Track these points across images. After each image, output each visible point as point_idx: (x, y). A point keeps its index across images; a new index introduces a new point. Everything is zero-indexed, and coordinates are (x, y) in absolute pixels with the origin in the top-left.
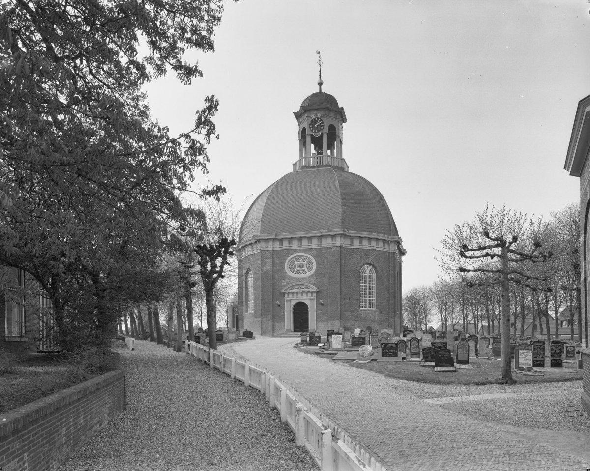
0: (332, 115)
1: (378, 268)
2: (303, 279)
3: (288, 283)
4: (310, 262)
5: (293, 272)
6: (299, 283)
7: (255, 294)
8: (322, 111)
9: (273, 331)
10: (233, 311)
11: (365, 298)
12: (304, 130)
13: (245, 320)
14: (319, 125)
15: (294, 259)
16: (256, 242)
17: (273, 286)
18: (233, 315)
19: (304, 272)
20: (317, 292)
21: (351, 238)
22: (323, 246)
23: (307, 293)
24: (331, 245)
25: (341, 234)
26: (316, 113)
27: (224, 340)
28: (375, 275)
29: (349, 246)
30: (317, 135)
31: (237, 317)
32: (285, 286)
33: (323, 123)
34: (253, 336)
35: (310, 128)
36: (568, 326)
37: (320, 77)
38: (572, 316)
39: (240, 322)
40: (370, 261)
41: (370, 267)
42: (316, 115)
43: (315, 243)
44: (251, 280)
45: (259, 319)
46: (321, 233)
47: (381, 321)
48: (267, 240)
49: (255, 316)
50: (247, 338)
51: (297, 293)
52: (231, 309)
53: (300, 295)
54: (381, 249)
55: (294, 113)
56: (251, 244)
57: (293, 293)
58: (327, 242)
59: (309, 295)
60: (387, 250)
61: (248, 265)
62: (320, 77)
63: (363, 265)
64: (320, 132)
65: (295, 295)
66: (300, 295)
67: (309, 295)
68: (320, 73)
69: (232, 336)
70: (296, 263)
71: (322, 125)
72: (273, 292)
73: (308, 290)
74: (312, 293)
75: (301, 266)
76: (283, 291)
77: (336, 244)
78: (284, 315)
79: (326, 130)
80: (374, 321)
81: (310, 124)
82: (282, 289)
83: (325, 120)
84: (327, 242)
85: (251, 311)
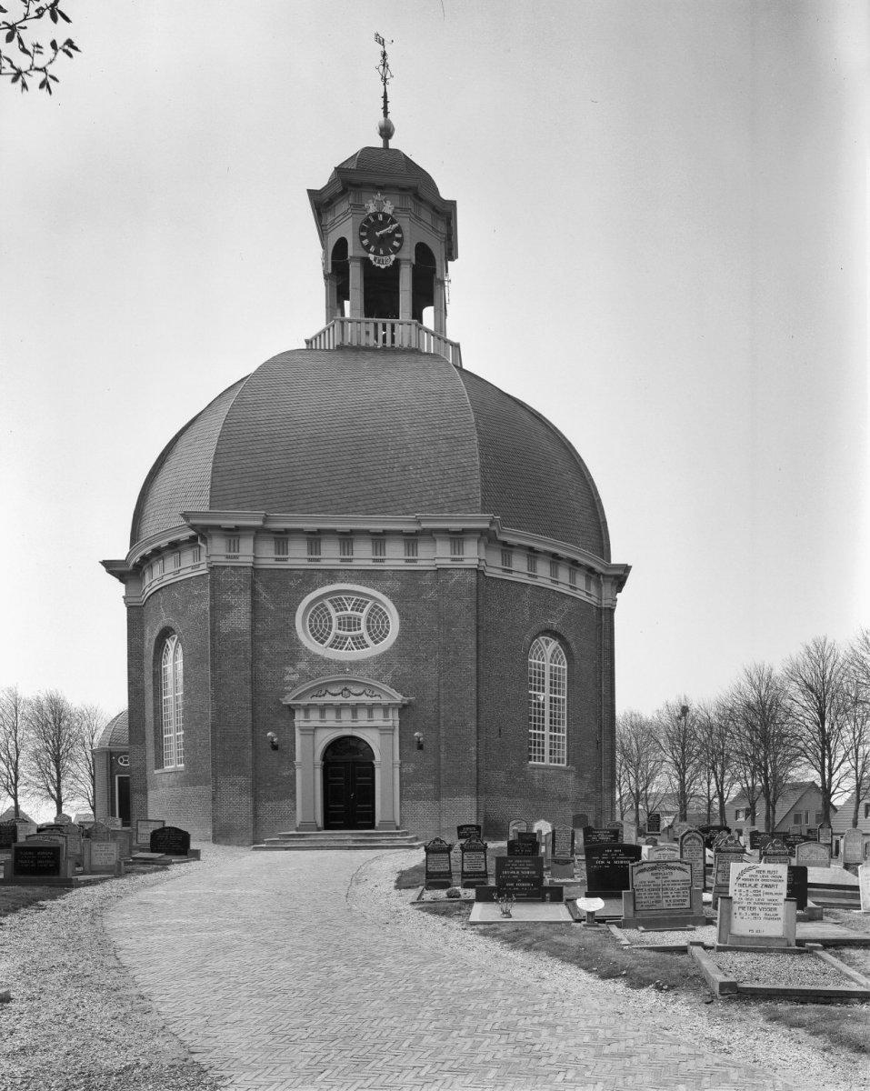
0: (426, 215)
1: (573, 646)
2: (356, 665)
3: (306, 676)
4: (377, 616)
5: (322, 642)
6: (345, 677)
7: (188, 709)
8: (397, 197)
9: (256, 826)
10: (112, 767)
11: (541, 732)
12: (341, 245)
13: (151, 794)
14: (390, 236)
15: (371, 602)
16: (193, 540)
17: (254, 681)
18: (111, 778)
19: (359, 643)
20: (403, 709)
21: (507, 549)
22: (422, 564)
23: (370, 708)
24: (447, 563)
25: (482, 532)
26: (378, 197)
27: (68, 868)
28: (566, 667)
29: (497, 574)
30: (385, 262)
31: (125, 784)
32: (295, 686)
33: (398, 230)
34: (193, 846)
35: (362, 238)
36: (746, 819)
37: (386, 113)
38: (753, 804)
39: (136, 799)
40: (554, 623)
41: (554, 644)
42: (380, 204)
43: (395, 555)
44: (174, 664)
45: (206, 790)
46: (419, 522)
47: (582, 800)
48: (234, 533)
49: (190, 778)
50: (168, 853)
51: (338, 709)
52: (102, 761)
53: (346, 715)
54: (582, 596)
55: (310, 192)
56: (175, 546)
57: (323, 709)
58: (435, 555)
59: (378, 715)
60: (593, 600)
61: (166, 619)
62: (386, 113)
63: (536, 637)
64: (393, 257)
65: (330, 715)
66: (346, 715)
67: (378, 715)
68: (386, 102)
69: (105, 853)
70: (334, 615)
71: (397, 235)
72: (254, 704)
73: (376, 700)
74: (386, 708)
75: (350, 623)
76: (288, 700)
77: (466, 562)
78: (293, 777)
79: (408, 253)
80: (566, 799)
81: (362, 229)
82: (284, 693)
83: (405, 222)
84: (435, 555)
85: (174, 764)
